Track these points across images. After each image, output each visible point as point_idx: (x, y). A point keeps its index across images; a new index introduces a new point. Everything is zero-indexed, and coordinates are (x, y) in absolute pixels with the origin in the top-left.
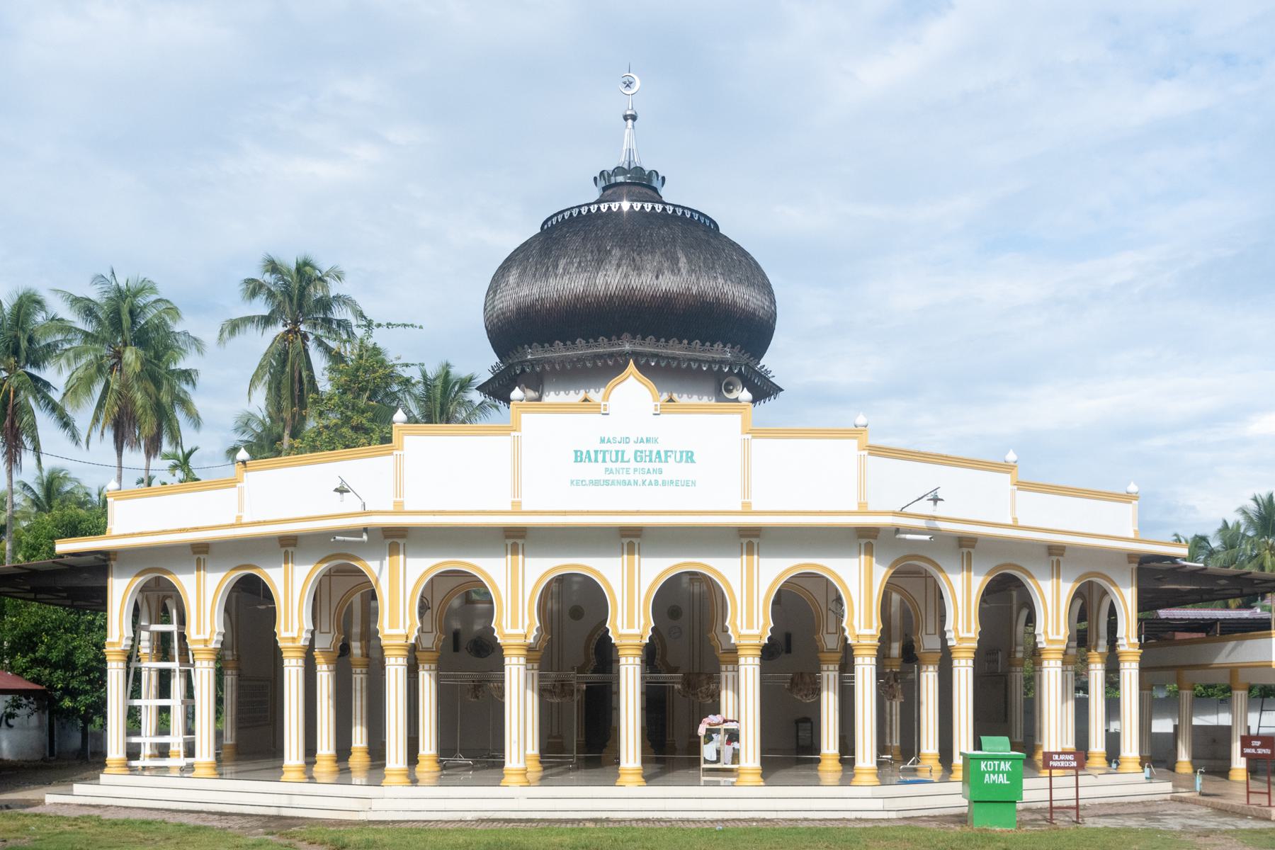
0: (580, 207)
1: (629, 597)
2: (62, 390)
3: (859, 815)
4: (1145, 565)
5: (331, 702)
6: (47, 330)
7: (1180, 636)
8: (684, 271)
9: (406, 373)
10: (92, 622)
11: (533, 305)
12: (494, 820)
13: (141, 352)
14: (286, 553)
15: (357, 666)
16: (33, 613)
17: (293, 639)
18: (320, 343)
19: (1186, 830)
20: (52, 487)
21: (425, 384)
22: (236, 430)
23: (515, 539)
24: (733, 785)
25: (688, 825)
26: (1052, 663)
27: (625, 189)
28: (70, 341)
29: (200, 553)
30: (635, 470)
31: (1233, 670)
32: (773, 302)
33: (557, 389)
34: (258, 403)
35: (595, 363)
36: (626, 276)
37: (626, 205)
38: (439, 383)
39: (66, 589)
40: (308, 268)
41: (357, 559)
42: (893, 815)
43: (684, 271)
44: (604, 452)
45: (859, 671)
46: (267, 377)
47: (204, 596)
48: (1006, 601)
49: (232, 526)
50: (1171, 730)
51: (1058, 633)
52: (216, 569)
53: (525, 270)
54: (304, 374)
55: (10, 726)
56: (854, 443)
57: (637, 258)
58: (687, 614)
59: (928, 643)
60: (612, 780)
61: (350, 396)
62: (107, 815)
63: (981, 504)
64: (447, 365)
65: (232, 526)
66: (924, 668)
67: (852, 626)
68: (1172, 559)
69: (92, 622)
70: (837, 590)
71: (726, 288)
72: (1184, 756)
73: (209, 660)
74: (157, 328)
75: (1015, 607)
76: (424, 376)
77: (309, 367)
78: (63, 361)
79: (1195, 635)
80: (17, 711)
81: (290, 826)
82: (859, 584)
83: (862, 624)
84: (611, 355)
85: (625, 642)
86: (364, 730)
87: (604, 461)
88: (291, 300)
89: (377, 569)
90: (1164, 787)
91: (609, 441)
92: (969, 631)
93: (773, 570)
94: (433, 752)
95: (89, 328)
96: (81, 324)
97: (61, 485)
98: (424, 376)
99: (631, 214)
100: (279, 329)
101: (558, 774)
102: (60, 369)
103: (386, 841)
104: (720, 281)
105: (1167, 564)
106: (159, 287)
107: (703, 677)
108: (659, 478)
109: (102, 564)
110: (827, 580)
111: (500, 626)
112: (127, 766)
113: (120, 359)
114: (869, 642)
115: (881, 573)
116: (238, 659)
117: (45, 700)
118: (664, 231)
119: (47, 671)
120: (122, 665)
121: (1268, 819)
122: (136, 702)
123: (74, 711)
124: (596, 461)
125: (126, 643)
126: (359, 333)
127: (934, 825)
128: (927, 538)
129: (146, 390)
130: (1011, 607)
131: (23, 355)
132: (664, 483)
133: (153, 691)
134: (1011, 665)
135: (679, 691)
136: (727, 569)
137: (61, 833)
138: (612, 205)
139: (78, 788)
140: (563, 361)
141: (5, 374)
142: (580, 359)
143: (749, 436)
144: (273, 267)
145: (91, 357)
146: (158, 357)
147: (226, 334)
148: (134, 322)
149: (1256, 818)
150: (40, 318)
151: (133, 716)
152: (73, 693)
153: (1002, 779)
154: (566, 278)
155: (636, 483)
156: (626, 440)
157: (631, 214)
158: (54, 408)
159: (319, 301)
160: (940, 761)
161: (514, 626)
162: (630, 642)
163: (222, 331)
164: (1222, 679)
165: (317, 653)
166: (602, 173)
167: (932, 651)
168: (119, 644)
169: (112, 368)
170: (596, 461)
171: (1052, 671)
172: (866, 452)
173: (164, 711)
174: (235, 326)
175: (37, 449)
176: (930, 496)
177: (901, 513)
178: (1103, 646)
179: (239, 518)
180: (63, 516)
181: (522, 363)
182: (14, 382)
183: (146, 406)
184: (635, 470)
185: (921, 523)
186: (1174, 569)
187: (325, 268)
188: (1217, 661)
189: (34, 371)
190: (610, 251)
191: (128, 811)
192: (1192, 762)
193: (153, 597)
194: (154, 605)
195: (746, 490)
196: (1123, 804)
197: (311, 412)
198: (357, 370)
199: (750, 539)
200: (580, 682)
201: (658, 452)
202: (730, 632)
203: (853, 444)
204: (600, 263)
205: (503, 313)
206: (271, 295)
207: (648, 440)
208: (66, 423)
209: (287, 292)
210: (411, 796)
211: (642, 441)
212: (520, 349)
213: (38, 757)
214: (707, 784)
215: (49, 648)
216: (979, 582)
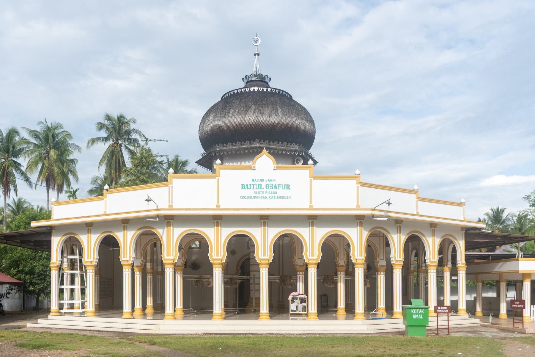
0: (237, 89)
1: (264, 244)
2: (25, 166)
3: (358, 332)
4: (468, 232)
5: (141, 287)
6: (20, 143)
7: (476, 261)
8: (280, 115)
9: (159, 159)
10: (41, 256)
11: (219, 128)
12: (210, 334)
13: (57, 152)
14: (124, 226)
15: (149, 273)
16: (18, 252)
17: (127, 261)
18: (127, 148)
19: (494, 338)
20: (19, 207)
21: (168, 163)
22: (91, 183)
23: (217, 220)
24: (305, 320)
25: (301, 336)
26: (432, 271)
27: (255, 83)
28: (29, 147)
29: (89, 227)
30: (266, 192)
31: (500, 274)
32: (314, 127)
33: (229, 162)
34: (102, 172)
35: (245, 151)
36: (257, 116)
37: (256, 89)
38: (174, 163)
39: (35, 242)
40: (122, 118)
41: (153, 228)
42: (372, 332)
43: (280, 115)
44: (254, 185)
45: (357, 274)
46: (106, 161)
47: (90, 243)
48: (414, 246)
49: (103, 215)
50: (473, 299)
51: (434, 259)
52: (95, 233)
53: (216, 114)
54: (120, 160)
55: (8, 298)
56: (355, 181)
57: (262, 110)
58: (287, 251)
59: (382, 263)
60: (257, 318)
61: (139, 168)
62: (53, 332)
63: (405, 206)
64: (177, 156)
65: (103, 215)
66: (379, 273)
67: (354, 255)
68: (479, 229)
69: (41, 256)
70: (348, 241)
71: (297, 121)
72: (479, 309)
73: (93, 269)
74: (63, 142)
75: (410, 249)
76: (168, 160)
77: (122, 157)
78: (26, 155)
79: (482, 261)
80: (11, 291)
81: (129, 336)
82: (357, 238)
83: (358, 255)
84: (251, 148)
85: (262, 262)
86: (152, 299)
87: (253, 189)
88: (115, 131)
89: (162, 232)
90: (476, 321)
91: (255, 181)
92: (400, 258)
93: (322, 233)
94: (182, 307)
95: (36, 142)
96: (33, 141)
97: (23, 204)
98: (168, 160)
99: (258, 92)
100: (111, 142)
101: (231, 316)
102: (25, 158)
103: (171, 341)
104: (295, 118)
105: (477, 231)
106: (64, 126)
107: (288, 277)
108: (276, 195)
109: (49, 231)
110: (344, 237)
111: (211, 255)
112: (59, 312)
113: (48, 154)
114: (361, 262)
115: (366, 234)
116: (100, 270)
117: (22, 287)
118: (272, 99)
119: (24, 275)
120: (57, 272)
121: (525, 333)
122: (62, 287)
123: (34, 291)
124: (250, 189)
125: (59, 263)
126: (142, 143)
127: (390, 336)
128: (386, 219)
129: (59, 167)
130: (409, 249)
131: (11, 153)
132: (278, 198)
133: (69, 282)
134: (408, 273)
135: (278, 283)
136: (304, 233)
137: (37, 338)
138: (251, 89)
139: (40, 321)
140: (231, 151)
141: (3, 160)
142: (238, 150)
143: (312, 179)
144: (108, 118)
145: (37, 153)
146: (62, 154)
147: (90, 144)
148: (54, 140)
149: (519, 333)
150: (17, 138)
151: (61, 291)
152: (31, 284)
153: (420, 317)
154: (233, 117)
155: (266, 197)
156: (262, 180)
157: (258, 92)
158: (23, 173)
159: (126, 131)
160: (386, 310)
161: (217, 255)
162: (264, 262)
163: (88, 143)
164: (496, 278)
165: (135, 267)
166: (246, 76)
167: (382, 266)
168: (56, 263)
169: (45, 158)
170: (250, 189)
171: (432, 274)
172: (359, 185)
173: (72, 291)
174: (93, 141)
175: (16, 189)
176: (387, 202)
177: (374, 210)
178: (450, 265)
179: (105, 212)
180: (29, 214)
181: (215, 151)
182: (7, 163)
183: (58, 173)
184: (266, 192)
185: (382, 214)
186: (479, 233)
187: (129, 118)
188: (494, 270)
189: (15, 159)
190: (251, 107)
191: (61, 330)
192: (482, 312)
193: (69, 244)
194: (69, 248)
195: (311, 200)
196: (462, 328)
197: (123, 175)
198: (142, 158)
199: (312, 220)
200: (238, 278)
201: (275, 185)
202: (304, 258)
203: (354, 182)
204: (246, 111)
205: (207, 132)
206: (108, 129)
207: (271, 180)
208: (27, 180)
209: (114, 128)
210: (175, 324)
211: (269, 180)
212: (214, 146)
213: (18, 310)
214: (292, 320)
215: (24, 266)
216: (403, 238)
